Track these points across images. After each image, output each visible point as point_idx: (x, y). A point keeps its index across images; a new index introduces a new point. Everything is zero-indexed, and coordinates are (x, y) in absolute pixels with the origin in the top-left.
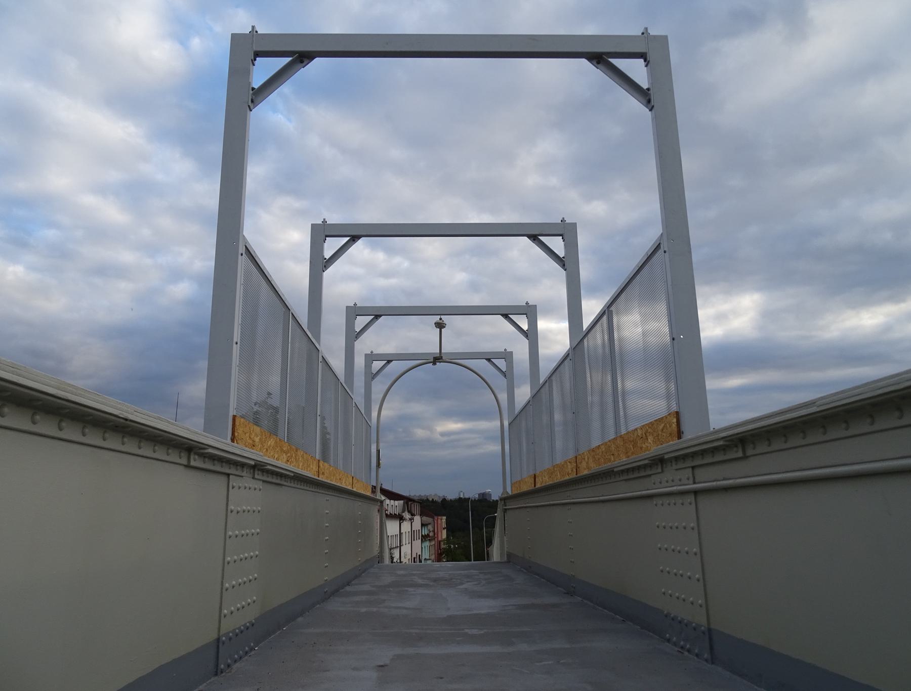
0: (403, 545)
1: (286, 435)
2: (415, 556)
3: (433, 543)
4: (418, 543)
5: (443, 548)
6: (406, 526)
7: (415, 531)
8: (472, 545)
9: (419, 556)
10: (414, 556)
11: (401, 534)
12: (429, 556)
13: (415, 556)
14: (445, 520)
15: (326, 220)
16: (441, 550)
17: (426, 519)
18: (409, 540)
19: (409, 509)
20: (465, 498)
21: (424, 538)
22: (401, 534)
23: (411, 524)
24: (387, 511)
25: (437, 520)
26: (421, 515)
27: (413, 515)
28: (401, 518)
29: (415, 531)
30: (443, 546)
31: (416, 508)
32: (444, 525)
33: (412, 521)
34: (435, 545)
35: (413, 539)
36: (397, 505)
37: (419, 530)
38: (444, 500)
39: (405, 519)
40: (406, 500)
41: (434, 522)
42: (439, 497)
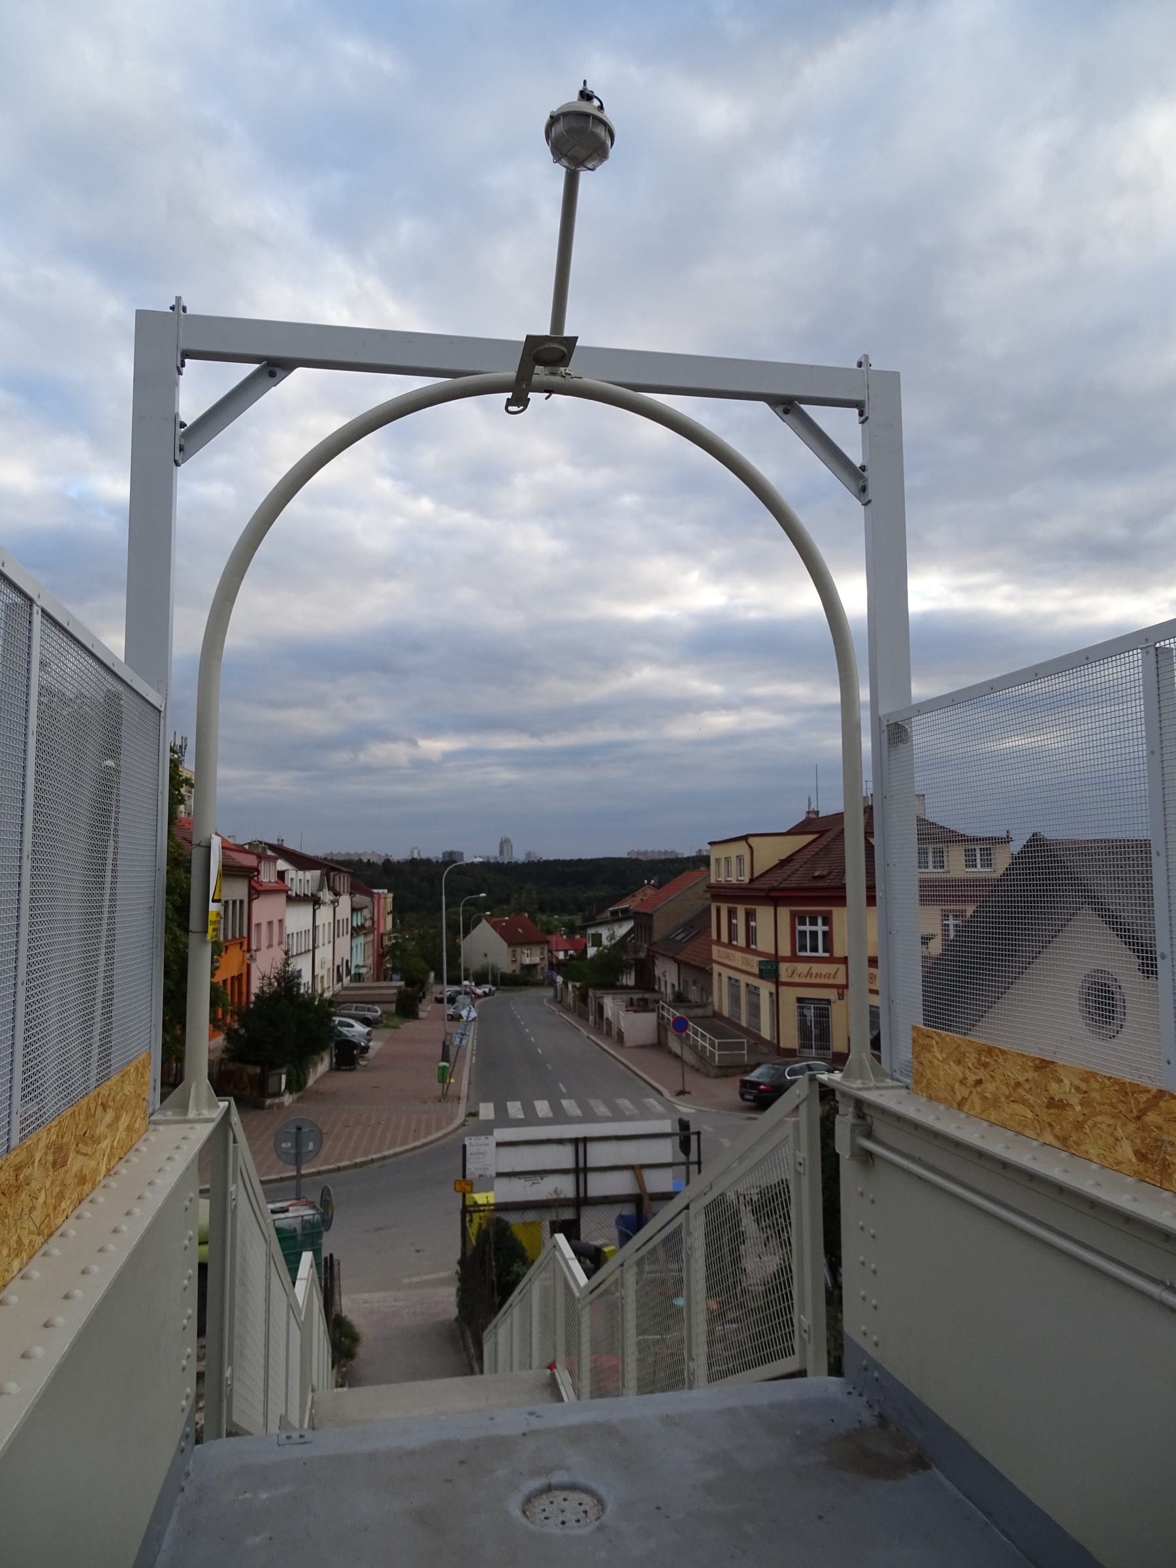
0: (318, 946)
1: (28, 847)
3: (370, 938)
4: (344, 941)
5: (387, 946)
6: (325, 915)
7: (345, 933)
8: (445, 954)
9: (347, 962)
10: (338, 962)
11: (315, 927)
12: (364, 960)
14: (391, 900)
15: (185, 302)
16: (383, 948)
17: (360, 899)
18: (329, 936)
19: (331, 885)
20: (421, 860)
21: (356, 931)
22: (315, 927)
24: (291, 890)
25: (379, 900)
26: (351, 894)
27: (337, 894)
28: (316, 902)
29: (345, 933)
30: (387, 942)
31: (343, 882)
32: (389, 908)
33: (336, 904)
34: (373, 941)
35: (336, 934)
36: (310, 879)
37: (347, 919)
38: (387, 862)
39: (324, 903)
40: (325, 870)
41: (374, 903)
42: (379, 855)
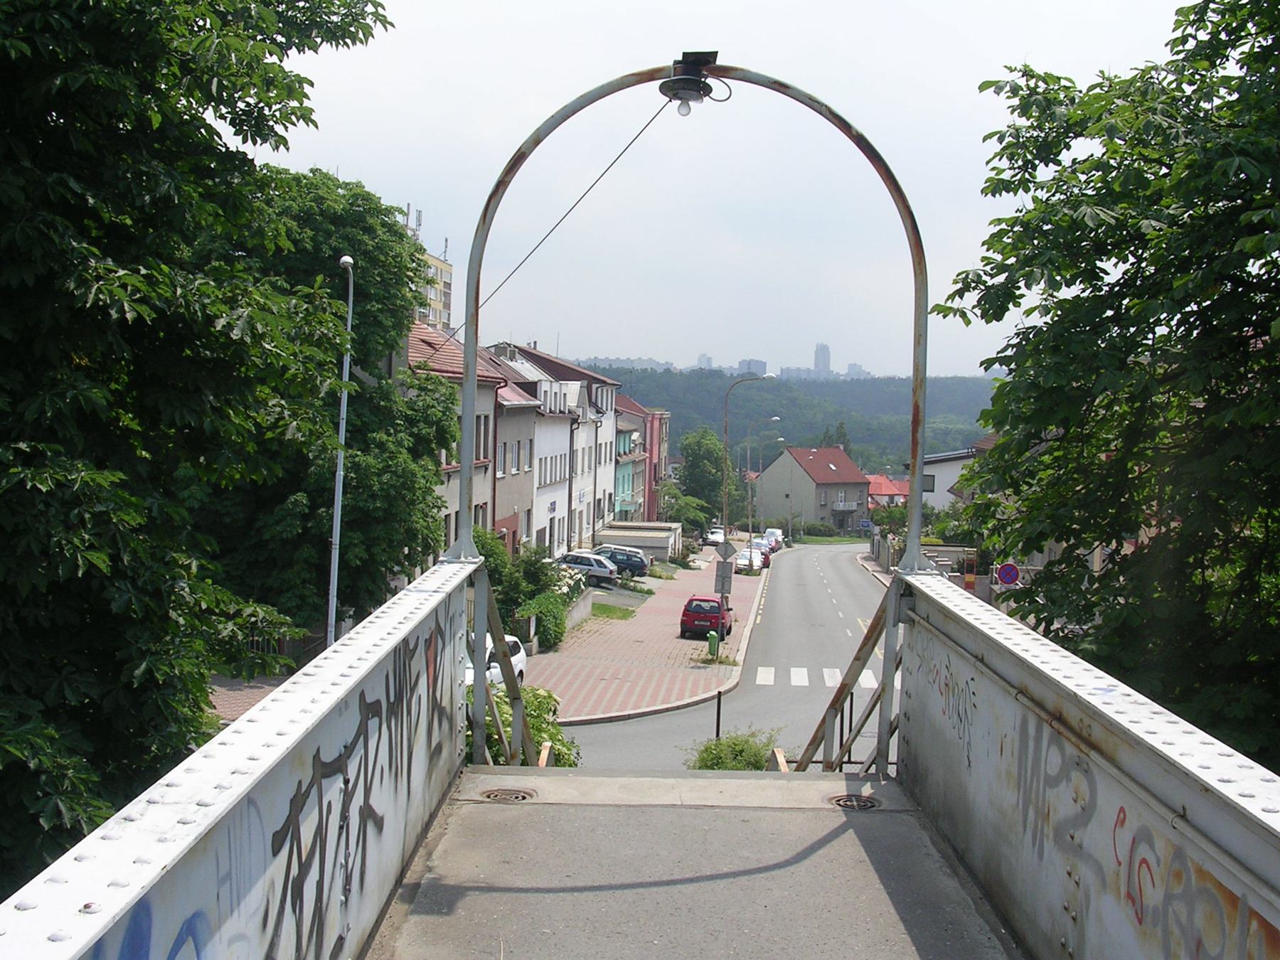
2: (601, 497)
6: (583, 438)
13: (601, 497)
19: (593, 400)
22: (572, 452)
23: (572, 432)
31: (606, 398)
37: (611, 443)
41: (646, 425)
